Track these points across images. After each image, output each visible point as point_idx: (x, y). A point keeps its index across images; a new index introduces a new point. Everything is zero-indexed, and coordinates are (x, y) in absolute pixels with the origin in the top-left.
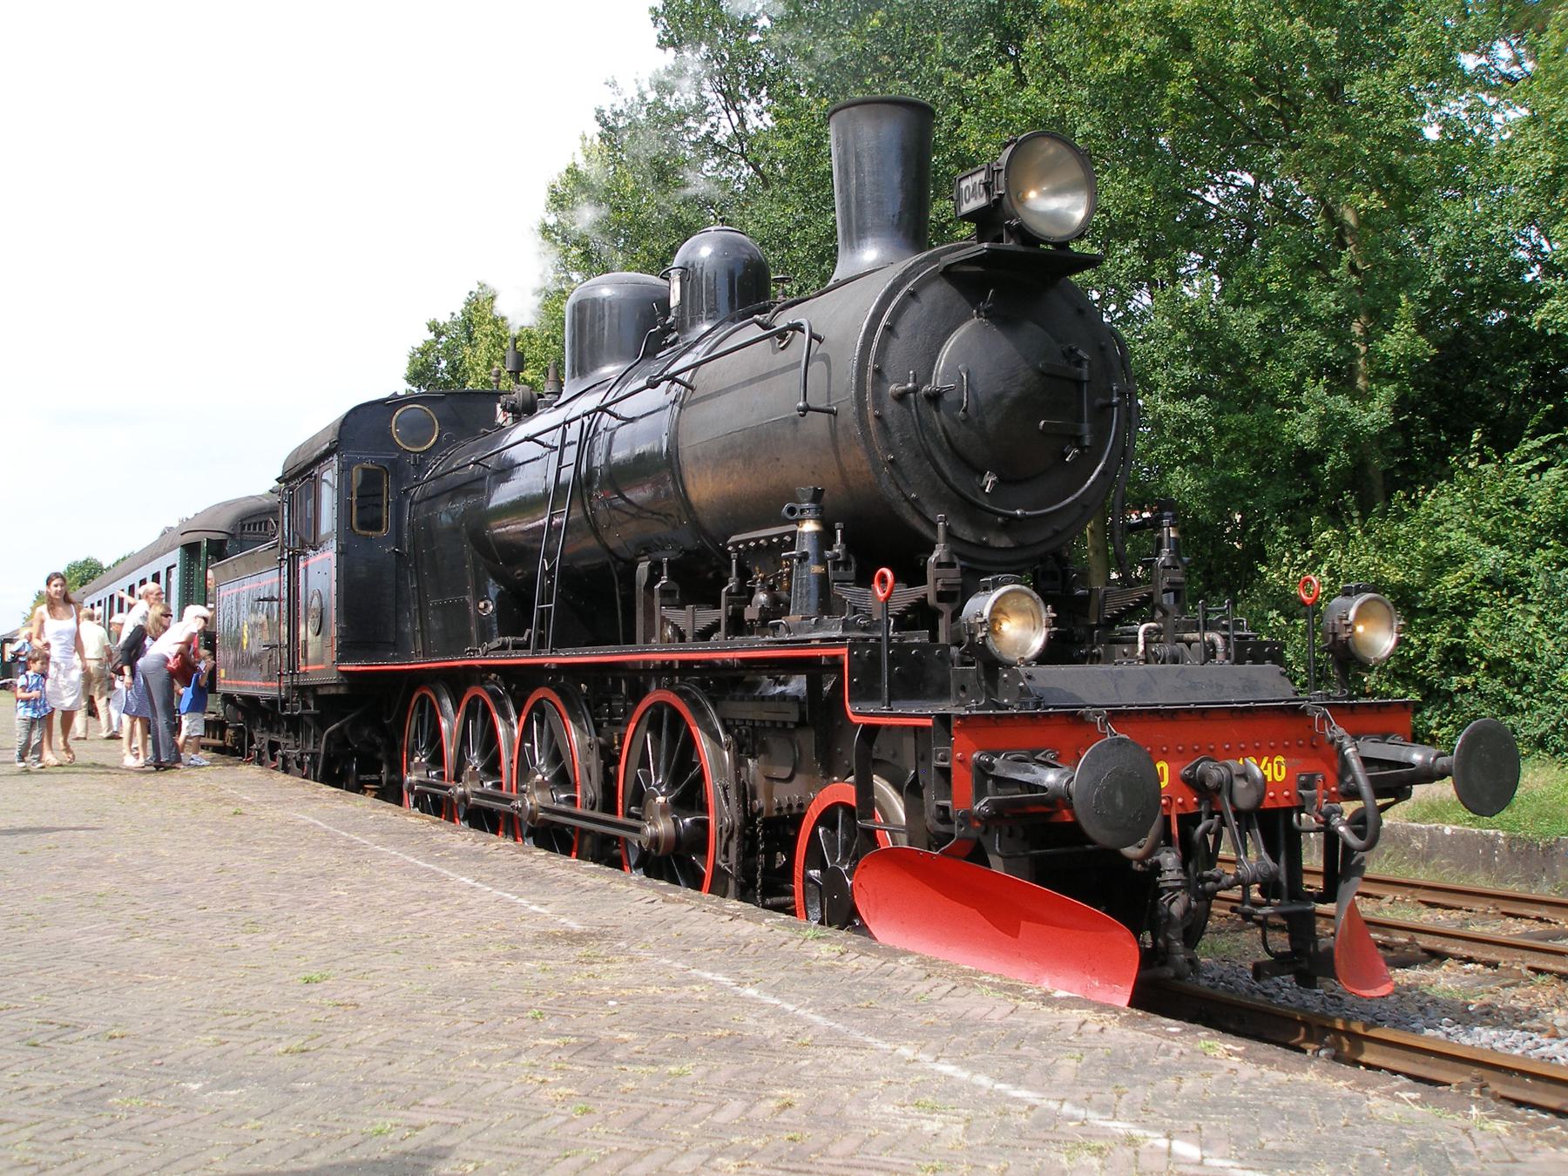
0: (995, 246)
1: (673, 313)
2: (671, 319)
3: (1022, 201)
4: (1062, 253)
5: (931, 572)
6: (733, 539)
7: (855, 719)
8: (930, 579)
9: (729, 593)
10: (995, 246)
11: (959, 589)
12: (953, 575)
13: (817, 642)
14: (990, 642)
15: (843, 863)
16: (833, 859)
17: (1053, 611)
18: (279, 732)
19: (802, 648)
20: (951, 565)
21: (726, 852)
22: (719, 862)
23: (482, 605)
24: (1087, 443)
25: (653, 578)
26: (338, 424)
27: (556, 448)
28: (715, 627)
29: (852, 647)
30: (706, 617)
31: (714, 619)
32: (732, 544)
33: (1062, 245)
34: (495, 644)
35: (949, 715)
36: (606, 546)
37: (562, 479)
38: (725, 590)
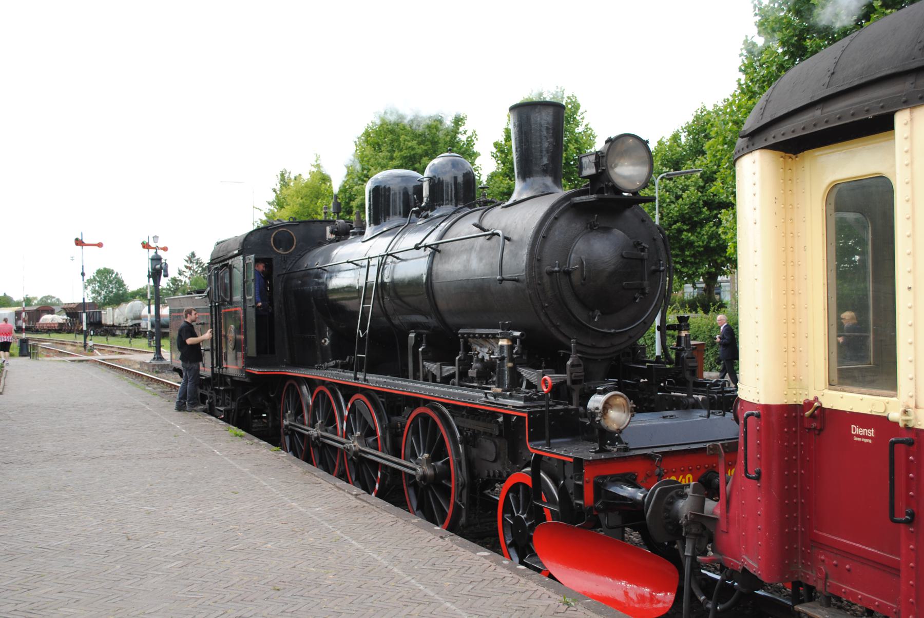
0: (600, 196)
1: (425, 200)
2: (423, 204)
3: (621, 182)
4: (636, 197)
5: (568, 369)
6: (461, 331)
7: (532, 450)
8: (568, 372)
9: (459, 360)
10: (600, 196)
11: (583, 378)
12: (580, 371)
13: (511, 408)
14: (602, 422)
15: (523, 514)
16: (518, 513)
17: (634, 403)
18: (206, 390)
19: (502, 408)
20: (579, 365)
21: (461, 495)
22: (457, 501)
23: (323, 341)
24: (647, 291)
25: (417, 344)
26: (245, 236)
27: (365, 267)
28: (452, 376)
29: (529, 413)
30: (448, 370)
31: (452, 371)
32: (461, 333)
33: (635, 193)
34: (332, 363)
35: (582, 459)
36: (392, 324)
37: (369, 280)
38: (457, 358)
